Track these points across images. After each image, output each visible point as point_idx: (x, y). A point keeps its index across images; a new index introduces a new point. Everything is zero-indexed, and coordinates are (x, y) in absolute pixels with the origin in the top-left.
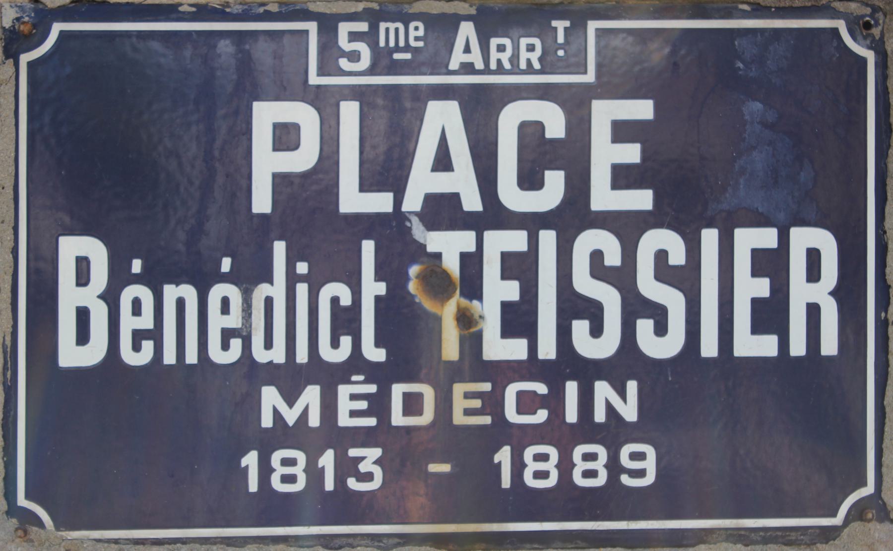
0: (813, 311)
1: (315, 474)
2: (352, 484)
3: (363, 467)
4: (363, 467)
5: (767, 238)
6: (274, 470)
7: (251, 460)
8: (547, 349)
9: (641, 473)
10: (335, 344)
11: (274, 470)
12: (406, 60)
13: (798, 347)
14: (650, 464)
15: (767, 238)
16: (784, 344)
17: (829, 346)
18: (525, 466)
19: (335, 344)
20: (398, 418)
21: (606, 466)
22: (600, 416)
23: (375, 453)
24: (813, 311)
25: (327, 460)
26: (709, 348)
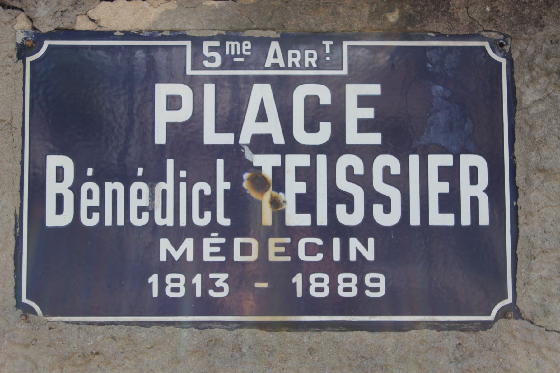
0: (474, 201)
1: (190, 287)
2: (211, 293)
3: (218, 284)
4: (218, 284)
5: (447, 160)
6: (167, 285)
7: (154, 279)
10: (202, 216)
11: (167, 285)
13: (466, 221)
14: (382, 285)
15: (447, 160)
16: (458, 218)
17: (484, 220)
19: (202, 216)
24: (474, 201)
25: (197, 280)
26: (415, 220)
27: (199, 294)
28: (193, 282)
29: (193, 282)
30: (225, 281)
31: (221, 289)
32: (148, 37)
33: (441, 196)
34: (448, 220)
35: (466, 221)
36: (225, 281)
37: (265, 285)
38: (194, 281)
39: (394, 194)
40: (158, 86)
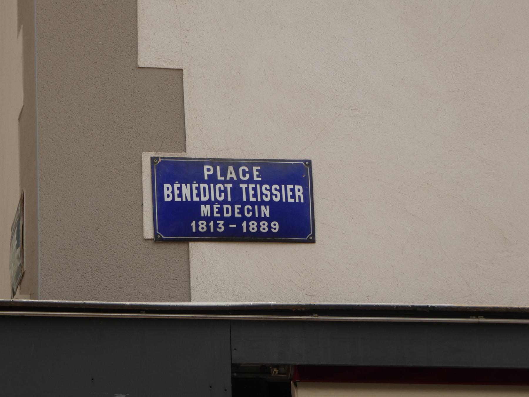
0: (299, 197)
1: (208, 226)
2: (218, 229)
3: (219, 226)
4: (219, 226)
5: (292, 187)
6: (250, 226)
7: (193, 224)
8: (259, 200)
9: (275, 229)
10: (220, 196)
11: (250, 226)
12: (255, 215)
13: (297, 201)
14: (277, 226)
15: (292, 187)
16: (295, 200)
17: (302, 201)
18: (256, 226)
19: (220, 196)
20: (225, 215)
21: (256, 226)
22: (263, 216)
23: (222, 222)
24: (299, 197)
25: (212, 224)
26: (284, 200)
27: (212, 230)
28: (242, 225)
29: (242, 225)
30: (223, 225)
31: (220, 228)
32: (471, 316)
33: (291, 195)
34: (293, 200)
35: (297, 201)
36: (223, 225)
37: (235, 226)
38: (210, 224)
39: (278, 193)
40: (255, 179)
